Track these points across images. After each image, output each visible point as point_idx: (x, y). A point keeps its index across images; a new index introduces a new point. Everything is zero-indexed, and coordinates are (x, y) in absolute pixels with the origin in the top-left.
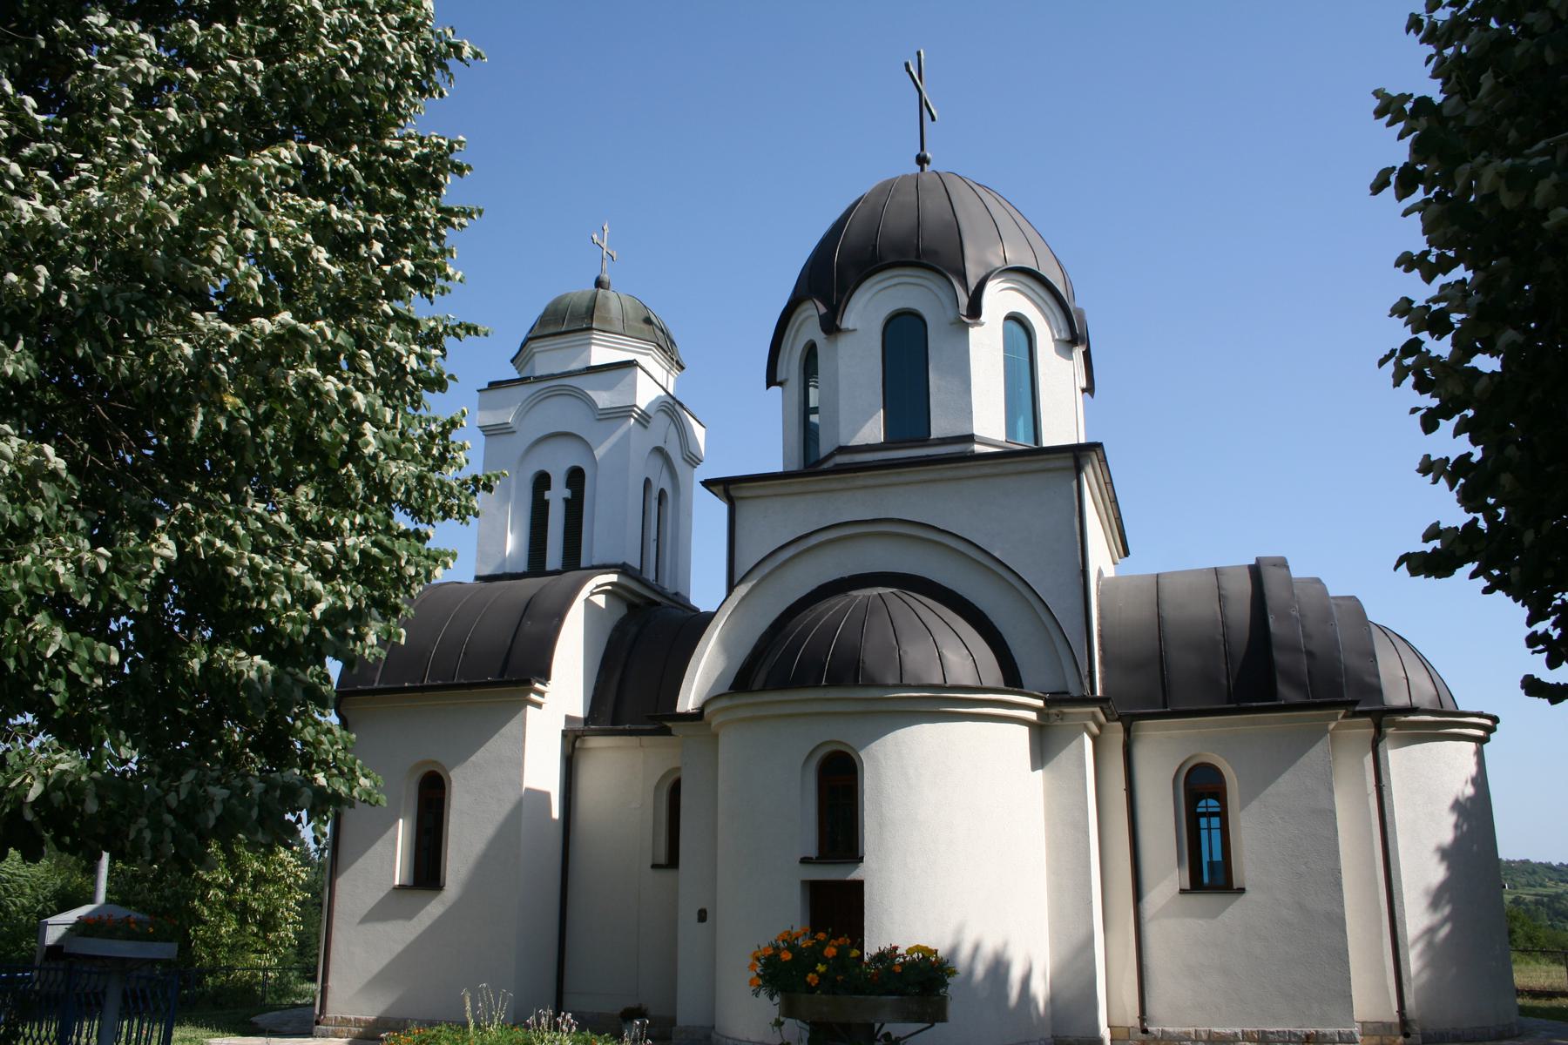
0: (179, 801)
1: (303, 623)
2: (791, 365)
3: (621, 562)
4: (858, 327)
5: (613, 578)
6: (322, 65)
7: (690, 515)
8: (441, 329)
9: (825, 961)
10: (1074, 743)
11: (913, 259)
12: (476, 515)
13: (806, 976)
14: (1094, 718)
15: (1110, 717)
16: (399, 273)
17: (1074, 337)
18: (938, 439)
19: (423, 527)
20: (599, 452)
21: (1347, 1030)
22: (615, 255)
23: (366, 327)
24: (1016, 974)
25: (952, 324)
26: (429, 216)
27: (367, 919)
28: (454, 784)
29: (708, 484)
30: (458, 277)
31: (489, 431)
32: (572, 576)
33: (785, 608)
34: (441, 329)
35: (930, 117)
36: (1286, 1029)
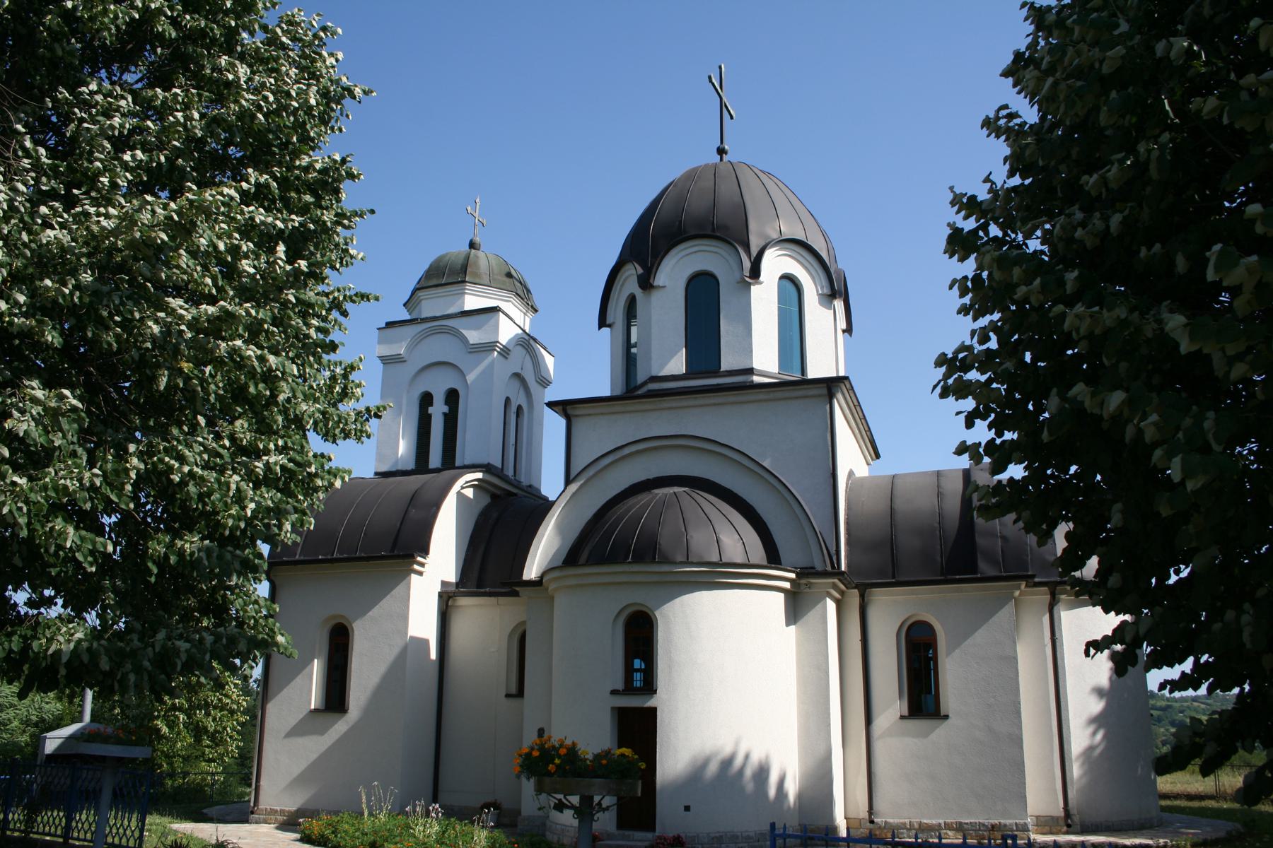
0: (154, 652)
1: (240, 520)
2: (617, 311)
3: (486, 463)
4: (667, 284)
5: (479, 475)
7: (541, 424)
8: (341, 299)
11: (709, 232)
12: (368, 437)
13: (548, 766)
14: (835, 587)
17: (836, 290)
18: (726, 371)
20: (470, 378)
21: (1022, 822)
25: (738, 283)
28: (356, 633)
29: (551, 405)
30: (360, 256)
31: (387, 360)
32: (448, 474)
33: (605, 501)
34: (341, 299)
36: (977, 821)
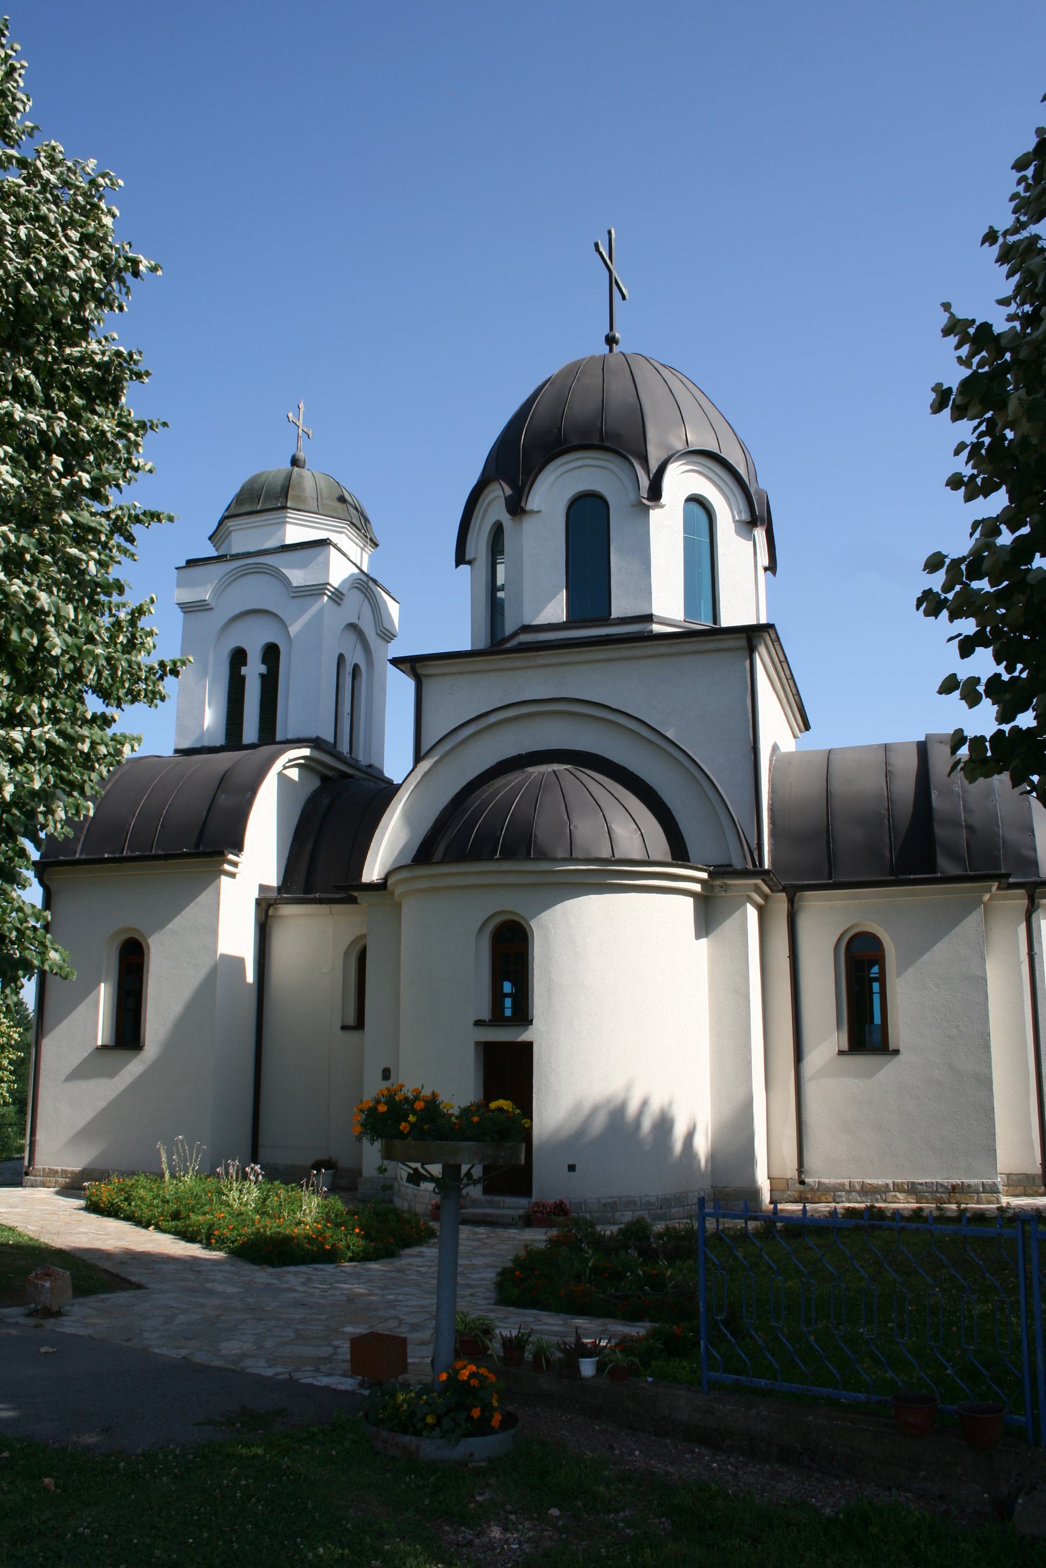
2: (479, 544)
3: (313, 735)
4: (542, 509)
5: (306, 752)
6: (8, 278)
9: (415, 1112)
10: (737, 913)
12: (163, 699)
14: (757, 889)
15: (773, 888)
16: (77, 485)
18: (618, 618)
19: (111, 711)
20: (294, 629)
22: (310, 433)
23: (47, 536)
24: (679, 1131)
25: (633, 506)
26: (108, 429)
27: (71, 1077)
28: (152, 950)
29: (396, 662)
30: (147, 468)
31: (188, 608)
35: (620, 297)
36: (934, 1181)
